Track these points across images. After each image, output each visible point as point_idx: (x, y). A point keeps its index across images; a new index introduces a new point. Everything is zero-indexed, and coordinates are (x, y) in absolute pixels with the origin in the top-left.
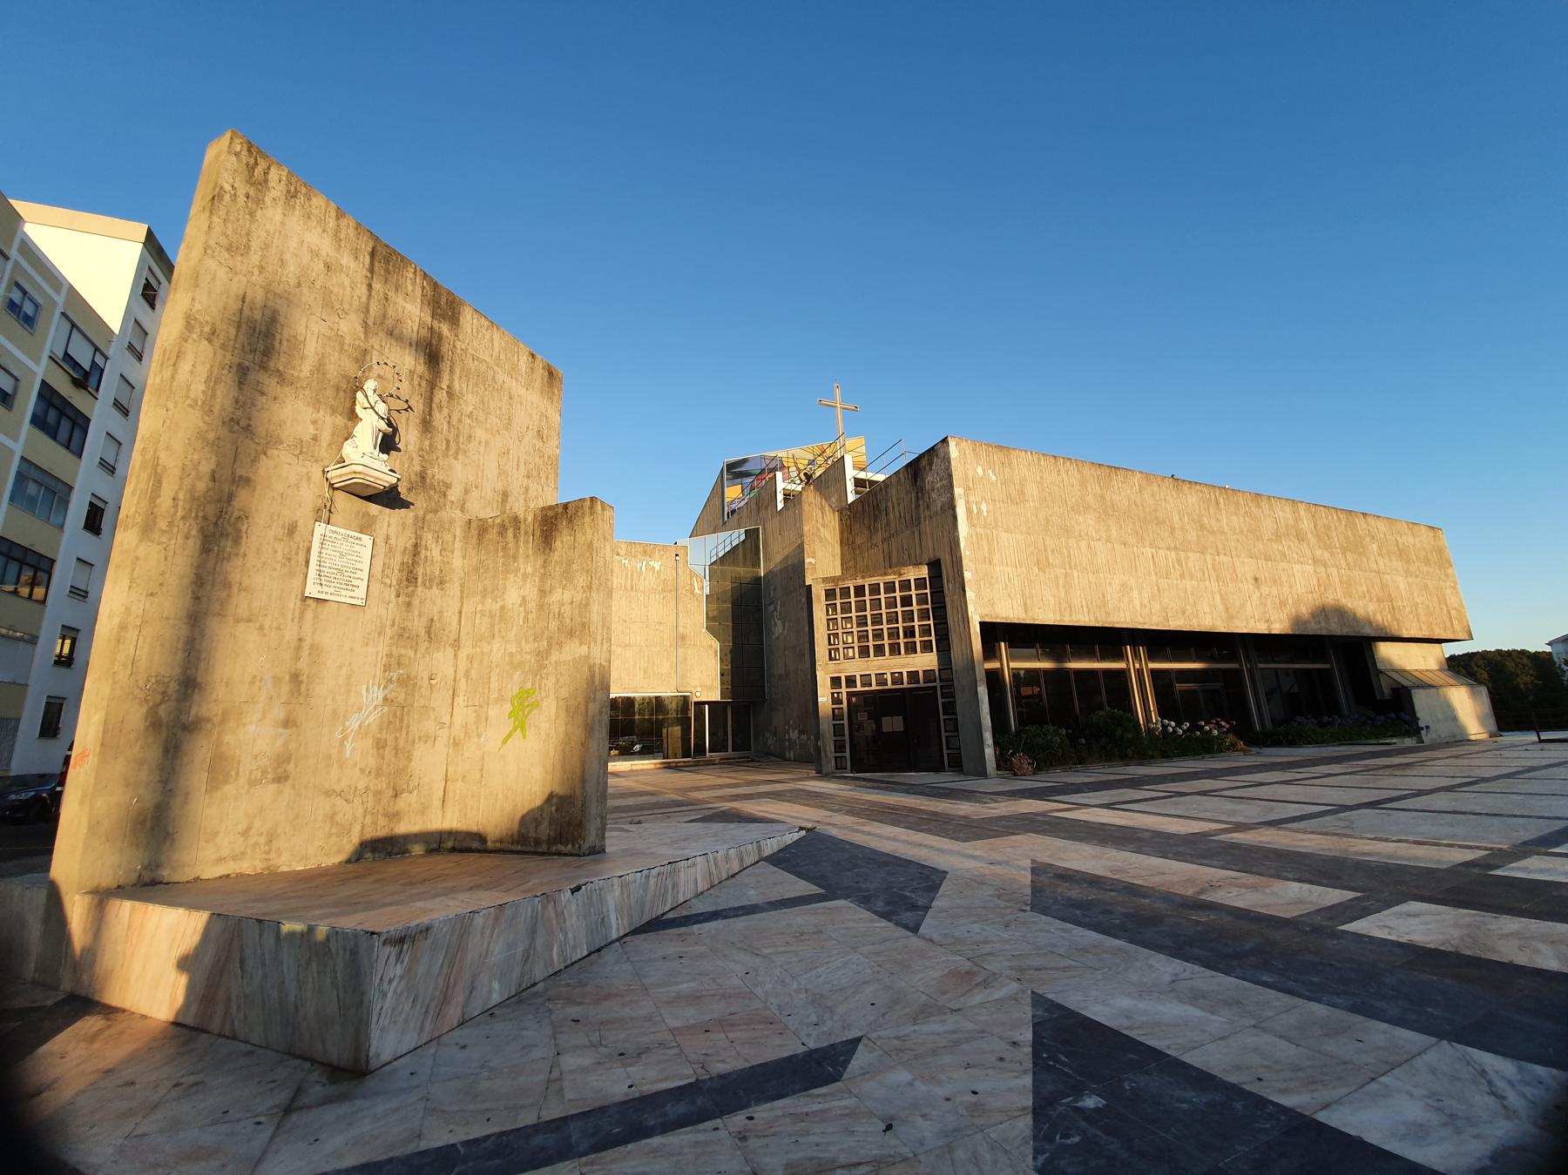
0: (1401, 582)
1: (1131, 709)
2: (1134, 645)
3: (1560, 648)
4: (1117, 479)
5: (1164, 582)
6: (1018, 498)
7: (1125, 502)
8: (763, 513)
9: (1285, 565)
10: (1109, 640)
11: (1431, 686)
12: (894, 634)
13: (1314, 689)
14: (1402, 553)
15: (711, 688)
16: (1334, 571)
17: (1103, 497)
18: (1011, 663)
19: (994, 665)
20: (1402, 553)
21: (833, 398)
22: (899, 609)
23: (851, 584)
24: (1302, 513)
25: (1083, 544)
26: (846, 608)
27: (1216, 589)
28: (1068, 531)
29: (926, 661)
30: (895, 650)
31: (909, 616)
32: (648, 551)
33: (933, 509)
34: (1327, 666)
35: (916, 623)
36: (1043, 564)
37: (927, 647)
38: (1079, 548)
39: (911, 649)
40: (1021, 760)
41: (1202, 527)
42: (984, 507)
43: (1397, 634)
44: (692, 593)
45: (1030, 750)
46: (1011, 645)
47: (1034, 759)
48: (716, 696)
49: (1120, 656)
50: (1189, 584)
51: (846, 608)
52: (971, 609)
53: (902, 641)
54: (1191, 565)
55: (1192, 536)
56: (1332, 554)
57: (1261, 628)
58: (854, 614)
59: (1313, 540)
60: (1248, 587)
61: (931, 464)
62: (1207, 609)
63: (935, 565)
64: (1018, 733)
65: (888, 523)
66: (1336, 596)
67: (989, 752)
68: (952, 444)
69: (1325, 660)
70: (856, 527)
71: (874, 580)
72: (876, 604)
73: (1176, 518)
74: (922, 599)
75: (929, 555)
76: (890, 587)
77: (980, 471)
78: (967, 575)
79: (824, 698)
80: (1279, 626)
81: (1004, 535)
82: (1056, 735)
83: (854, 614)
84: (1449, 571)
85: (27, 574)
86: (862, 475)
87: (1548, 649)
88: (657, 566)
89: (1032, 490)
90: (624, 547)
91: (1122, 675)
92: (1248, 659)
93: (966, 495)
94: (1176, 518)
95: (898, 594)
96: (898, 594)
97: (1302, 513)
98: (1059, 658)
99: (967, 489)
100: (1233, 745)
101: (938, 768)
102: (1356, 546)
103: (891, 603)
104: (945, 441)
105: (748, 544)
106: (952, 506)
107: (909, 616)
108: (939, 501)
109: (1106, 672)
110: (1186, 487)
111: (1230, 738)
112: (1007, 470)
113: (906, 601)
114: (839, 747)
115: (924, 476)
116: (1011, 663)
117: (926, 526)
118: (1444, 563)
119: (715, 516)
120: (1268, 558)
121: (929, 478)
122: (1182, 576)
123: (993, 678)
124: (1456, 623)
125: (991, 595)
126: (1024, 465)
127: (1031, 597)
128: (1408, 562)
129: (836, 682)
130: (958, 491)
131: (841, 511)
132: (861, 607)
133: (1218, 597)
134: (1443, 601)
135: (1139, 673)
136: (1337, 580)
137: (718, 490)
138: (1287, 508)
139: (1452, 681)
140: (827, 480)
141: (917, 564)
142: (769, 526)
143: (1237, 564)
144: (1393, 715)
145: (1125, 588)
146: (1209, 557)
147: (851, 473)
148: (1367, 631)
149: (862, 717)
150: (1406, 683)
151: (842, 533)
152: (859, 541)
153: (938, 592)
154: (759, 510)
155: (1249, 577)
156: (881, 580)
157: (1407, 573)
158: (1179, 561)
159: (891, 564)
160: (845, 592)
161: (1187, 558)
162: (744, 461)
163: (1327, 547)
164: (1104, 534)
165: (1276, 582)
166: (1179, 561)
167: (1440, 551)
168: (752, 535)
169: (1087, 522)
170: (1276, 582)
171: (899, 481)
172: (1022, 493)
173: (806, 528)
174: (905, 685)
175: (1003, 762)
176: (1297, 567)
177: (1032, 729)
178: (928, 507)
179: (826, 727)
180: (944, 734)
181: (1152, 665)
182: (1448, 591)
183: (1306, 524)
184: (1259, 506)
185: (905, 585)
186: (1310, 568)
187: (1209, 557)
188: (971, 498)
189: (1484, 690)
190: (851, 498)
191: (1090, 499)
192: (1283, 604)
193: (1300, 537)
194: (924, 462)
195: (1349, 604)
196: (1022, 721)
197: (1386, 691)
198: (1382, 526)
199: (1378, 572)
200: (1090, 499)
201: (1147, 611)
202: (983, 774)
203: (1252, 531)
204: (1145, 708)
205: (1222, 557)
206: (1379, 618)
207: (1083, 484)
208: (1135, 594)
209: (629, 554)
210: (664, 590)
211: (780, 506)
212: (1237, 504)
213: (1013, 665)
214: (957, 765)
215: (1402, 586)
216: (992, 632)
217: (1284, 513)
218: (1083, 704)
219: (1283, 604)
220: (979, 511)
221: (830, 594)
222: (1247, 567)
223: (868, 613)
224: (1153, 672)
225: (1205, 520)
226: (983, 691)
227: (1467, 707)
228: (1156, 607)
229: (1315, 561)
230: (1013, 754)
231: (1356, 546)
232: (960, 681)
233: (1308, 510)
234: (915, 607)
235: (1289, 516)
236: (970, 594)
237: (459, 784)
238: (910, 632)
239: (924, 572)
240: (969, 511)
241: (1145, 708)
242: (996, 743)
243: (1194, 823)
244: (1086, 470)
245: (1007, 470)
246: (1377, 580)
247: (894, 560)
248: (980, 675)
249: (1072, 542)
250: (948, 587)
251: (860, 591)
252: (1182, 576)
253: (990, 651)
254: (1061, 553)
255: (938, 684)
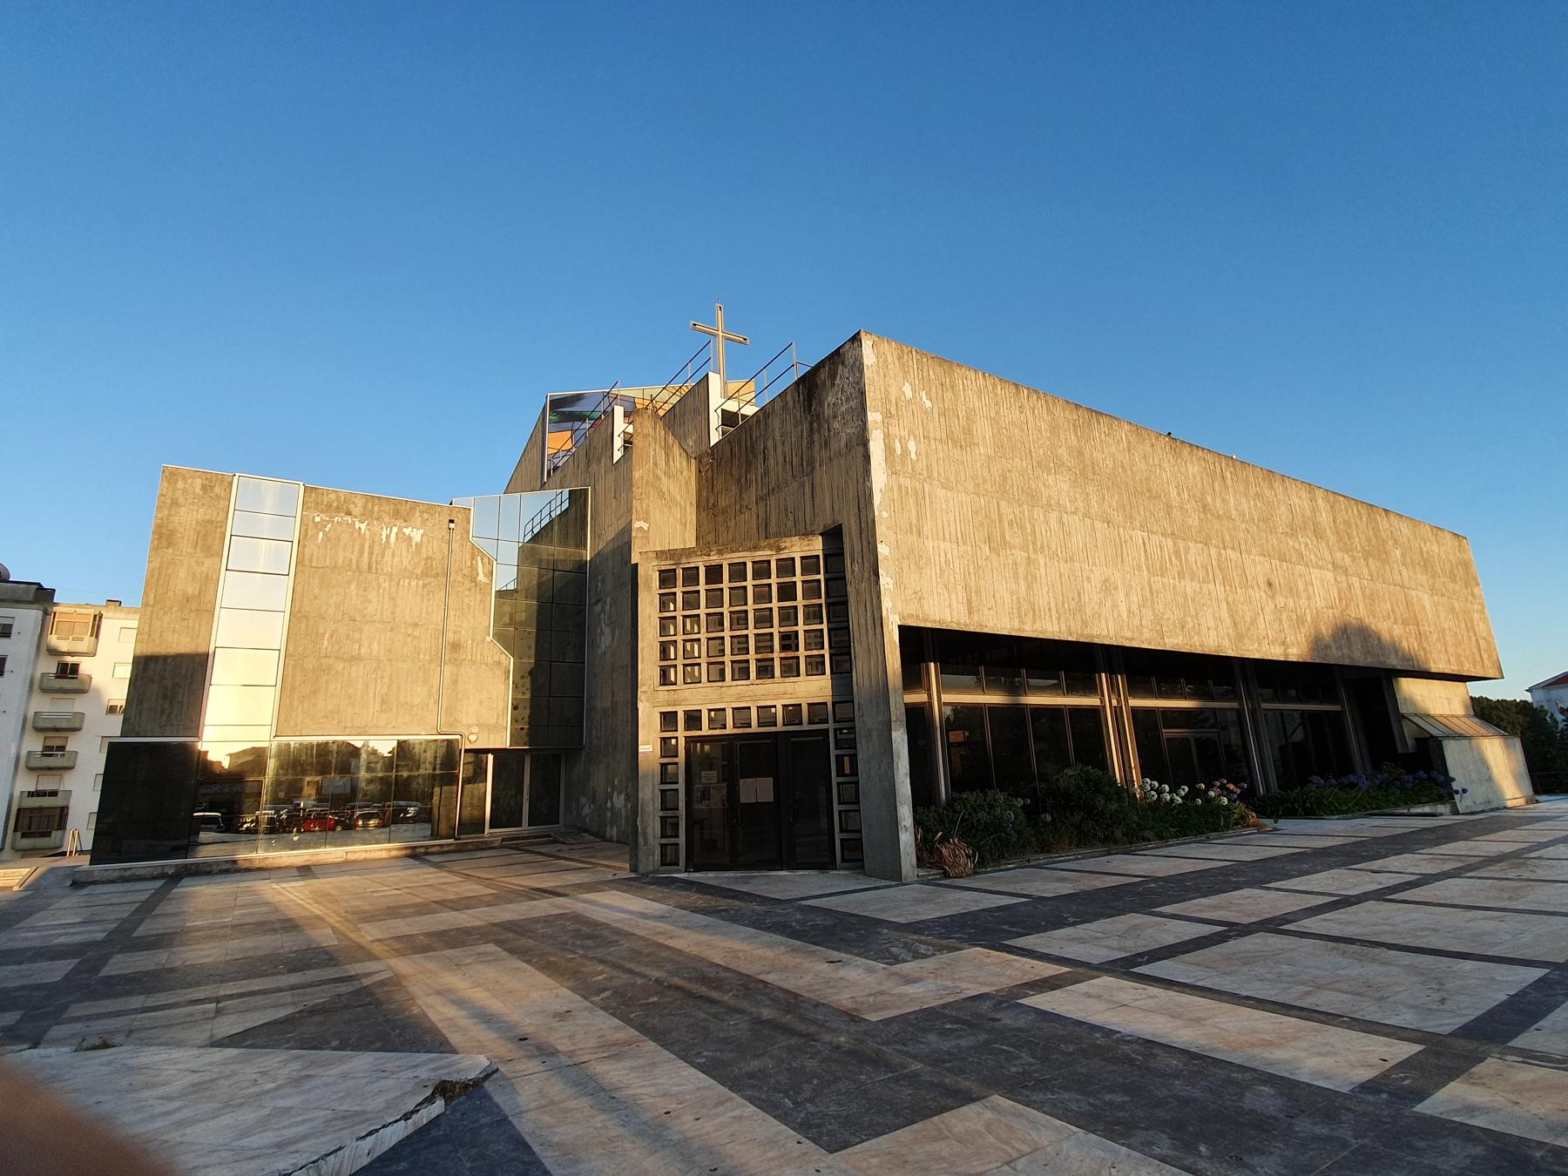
0: (1426, 598)
1: (1103, 764)
2: (1112, 673)
3: (1540, 694)
4: (1100, 429)
5: (1158, 581)
6: (963, 439)
7: (1109, 463)
8: (594, 466)
9: (1299, 568)
10: (1076, 661)
11: (1461, 736)
12: (764, 643)
13: (1329, 735)
14: (1426, 563)
15: (494, 728)
16: (1355, 580)
17: (1080, 453)
18: (947, 696)
19: (918, 697)
20: (1426, 563)
21: (713, 321)
22: (775, 604)
23: (701, 563)
24: (1320, 502)
25: (1053, 516)
26: (691, 601)
27: (1222, 596)
28: (1033, 497)
29: (814, 688)
30: (765, 671)
31: (789, 616)
32: (402, 512)
33: (834, 446)
34: (1336, 708)
35: (801, 628)
36: (997, 544)
37: (816, 666)
38: (1047, 522)
39: (791, 669)
40: (956, 851)
41: (1205, 508)
42: (912, 446)
43: (1424, 667)
44: (474, 580)
45: (970, 832)
46: (943, 670)
47: (977, 848)
48: (503, 740)
49: (1091, 688)
50: (1190, 586)
51: (691, 601)
52: (886, 604)
53: (777, 655)
54: (1191, 559)
55: (1194, 520)
56: (1354, 559)
57: (1275, 653)
58: (702, 611)
59: (1332, 539)
60: (1259, 595)
61: (833, 377)
62: (1211, 624)
63: (833, 536)
64: (951, 802)
65: (766, 473)
66: (1359, 612)
67: (907, 839)
68: (867, 343)
69: (1336, 701)
70: (719, 486)
71: (737, 557)
72: (739, 595)
73: (1173, 493)
74: (812, 589)
75: (825, 520)
76: (762, 570)
77: (907, 389)
78: (883, 550)
79: (649, 745)
80: (1296, 651)
81: (941, 492)
82: (1008, 809)
83: (702, 611)
84: (1476, 590)
85: (677, 696)
86: (732, 406)
87: (1528, 697)
88: (417, 535)
89: (983, 429)
90: (360, 502)
91: (1094, 714)
92: (1250, 697)
93: (886, 424)
94: (1173, 493)
95: (774, 580)
96: (774, 580)
97: (1320, 502)
98: (1013, 690)
99: (888, 415)
100: (1243, 817)
101: (824, 864)
102: (1377, 551)
103: (763, 595)
104: (856, 339)
105: (572, 514)
106: (862, 439)
107: (789, 616)
108: (843, 432)
109: (1076, 711)
110: (1186, 451)
111: (1240, 808)
112: (948, 395)
113: (787, 592)
114: (669, 828)
115: (822, 397)
116: (947, 696)
117: (822, 475)
118: (1471, 581)
119: (534, 472)
120: (1282, 559)
121: (831, 399)
122: (1181, 575)
123: (917, 718)
124: (1485, 656)
125: (923, 581)
126: (974, 392)
127: (978, 592)
128: (1433, 576)
129: (668, 719)
130: (873, 417)
131: (699, 459)
132: (715, 598)
133: (1224, 606)
134: (1470, 627)
135: (1117, 712)
136: (1359, 592)
137: (538, 440)
138: (1304, 494)
139: (1483, 731)
140: (685, 415)
141: (807, 534)
142: (600, 486)
143: (1247, 562)
144: (1421, 773)
145: (1107, 586)
146: (1213, 551)
147: (716, 400)
148: (1394, 662)
149: (710, 777)
150: (1434, 732)
151: (699, 492)
152: (723, 502)
153: (837, 579)
154: (588, 464)
155: (1262, 580)
156: (748, 558)
157: (1433, 591)
158: (1177, 553)
159: (768, 532)
160: (691, 576)
161: (1187, 550)
162: (578, 398)
163: (1347, 549)
164: (1081, 505)
165: (1293, 591)
166: (1177, 553)
167: (1466, 565)
168: (577, 498)
169: (1058, 486)
170: (1293, 591)
171: (785, 408)
172: (968, 431)
173: (637, 474)
174: (780, 727)
175: (927, 853)
176: (1316, 572)
177: (971, 797)
178: (826, 444)
179: (649, 793)
180: (836, 808)
181: (1134, 702)
182: (1476, 616)
183: (1324, 518)
184: (1271, 487)
185: (786, 566)
186: (1329, 576)
187: (1213, 551)
188: (893, 430)
189: (1517, 743)
190: (715, 437)
191: (1063, 452)
192: (1300, 620)
193: (1318, 534)
194: (823, 374)
195: (1369, 621)
196: (956, 784)
197: (1410, 742)
198: (1405, 528)
199: (1403, 587)
200: (1063, 452)
201: (1136, 621)
202: (893, 874)
203: (1265, 520)
204: (1123, 759)
205: (1229, 551)
206: (1405, 644)
207: (1054, 429)
208: (1121, 596)
209: (367, 515)
210: (425, 574)
211: (617, 455)
212: (1247, 481)
213: (946, 698)
214: (854, 858)
215: (1428, 607)
216: (922, 644)
217: (1299, 499)
218: (1066, 759)
219: (1300, 620)
220: (905, 451)
221: (667, 578)
222: (1259, 568)
223: (726, 610)
224: (1135, 712)
225: (1209, 500)
226: (900, 738)
227: (1499, 764)
228: (1148, 615)
229: (1335, 566)
230: (943, 840)
231: (1377, 551)
232: (866, 721)
233: (1326, 499)
234: (800, 602)
235: (1306, 504)
236: (886, 581)
237: (1290, 651)
238: (789, 641)
239: (816, 546)
240: (889, 450)
241: (1123, 759)
242: (917, 822)
243: (1107, 878)
244: (1058, 411)
245: (948, 395)
246: (1401, 597)
247: (773, 528)
248: (897, 713)
249: (1038, 513)
250: (853, 570)
251: (714, 573)
252: (1181, 575)
253: (913, 676)
254: (1022, 528)
255: (831, 726)
